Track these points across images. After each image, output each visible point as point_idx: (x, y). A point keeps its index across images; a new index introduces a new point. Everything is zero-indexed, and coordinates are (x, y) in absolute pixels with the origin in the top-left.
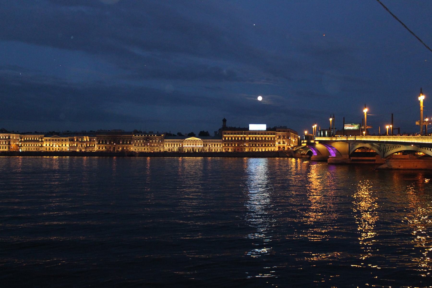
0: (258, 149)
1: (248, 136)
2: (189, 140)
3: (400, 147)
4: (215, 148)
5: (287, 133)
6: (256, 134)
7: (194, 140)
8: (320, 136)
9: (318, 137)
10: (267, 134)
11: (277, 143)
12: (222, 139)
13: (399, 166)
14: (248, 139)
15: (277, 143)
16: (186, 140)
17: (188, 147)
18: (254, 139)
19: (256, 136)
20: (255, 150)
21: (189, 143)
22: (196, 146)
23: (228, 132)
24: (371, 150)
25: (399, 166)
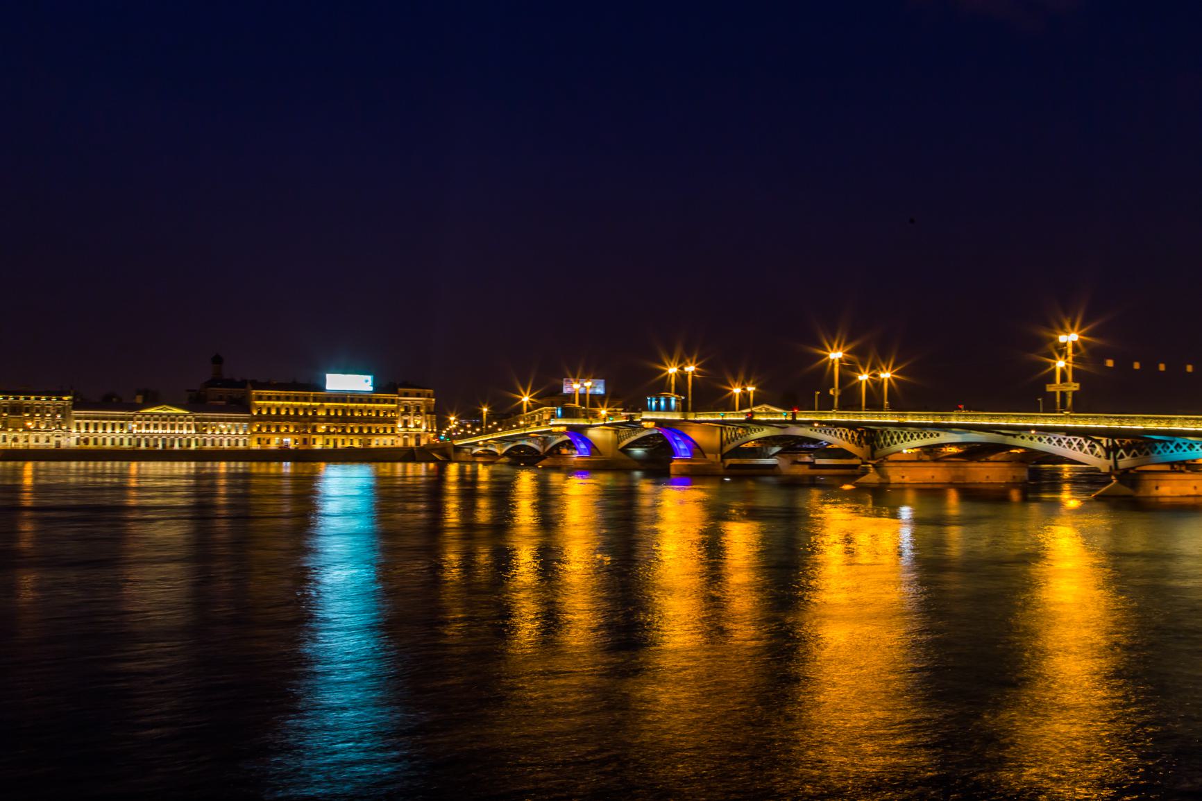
1: (323, 405)
2: (152, 414)
3: (938, 435)
4: (237, 438)
5: (426, 401)
6: (344, 400)
7: (169, 415)
8: (658, 409)
11: (400, 425)
12: (249, 411)
13: (903, 477)
14: (324, 414)
15: (400, 425)
16: (144, 415)
17: (158, 433)
18: (340, 414)
19: (345, 405)
20: (343, 444)
21: (152, 423)
22: (173, 431)
25: (903, 477)
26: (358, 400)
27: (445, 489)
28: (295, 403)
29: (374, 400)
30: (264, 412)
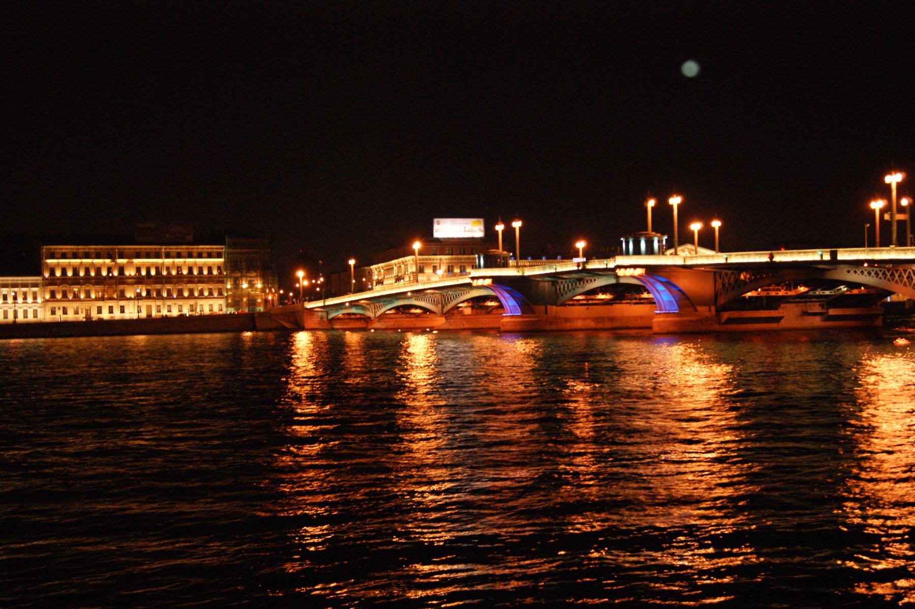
0: (98, 307)
1: (132, 263)
8: (637, 252)
9: (480, 267)
10: (93, 256)
12: (40, 273)
14: (133, 273)
18: (153, 273)
19: (159, 261)
20: (159, 311)
23: (64, 251)
24: (780, 291)
26: (175, 254)
27: (662, 342)
28: (96, 261)
29: (195, 254)
30: (58, 274)
